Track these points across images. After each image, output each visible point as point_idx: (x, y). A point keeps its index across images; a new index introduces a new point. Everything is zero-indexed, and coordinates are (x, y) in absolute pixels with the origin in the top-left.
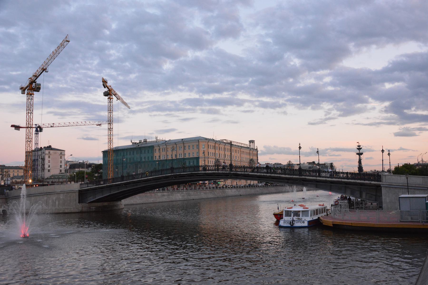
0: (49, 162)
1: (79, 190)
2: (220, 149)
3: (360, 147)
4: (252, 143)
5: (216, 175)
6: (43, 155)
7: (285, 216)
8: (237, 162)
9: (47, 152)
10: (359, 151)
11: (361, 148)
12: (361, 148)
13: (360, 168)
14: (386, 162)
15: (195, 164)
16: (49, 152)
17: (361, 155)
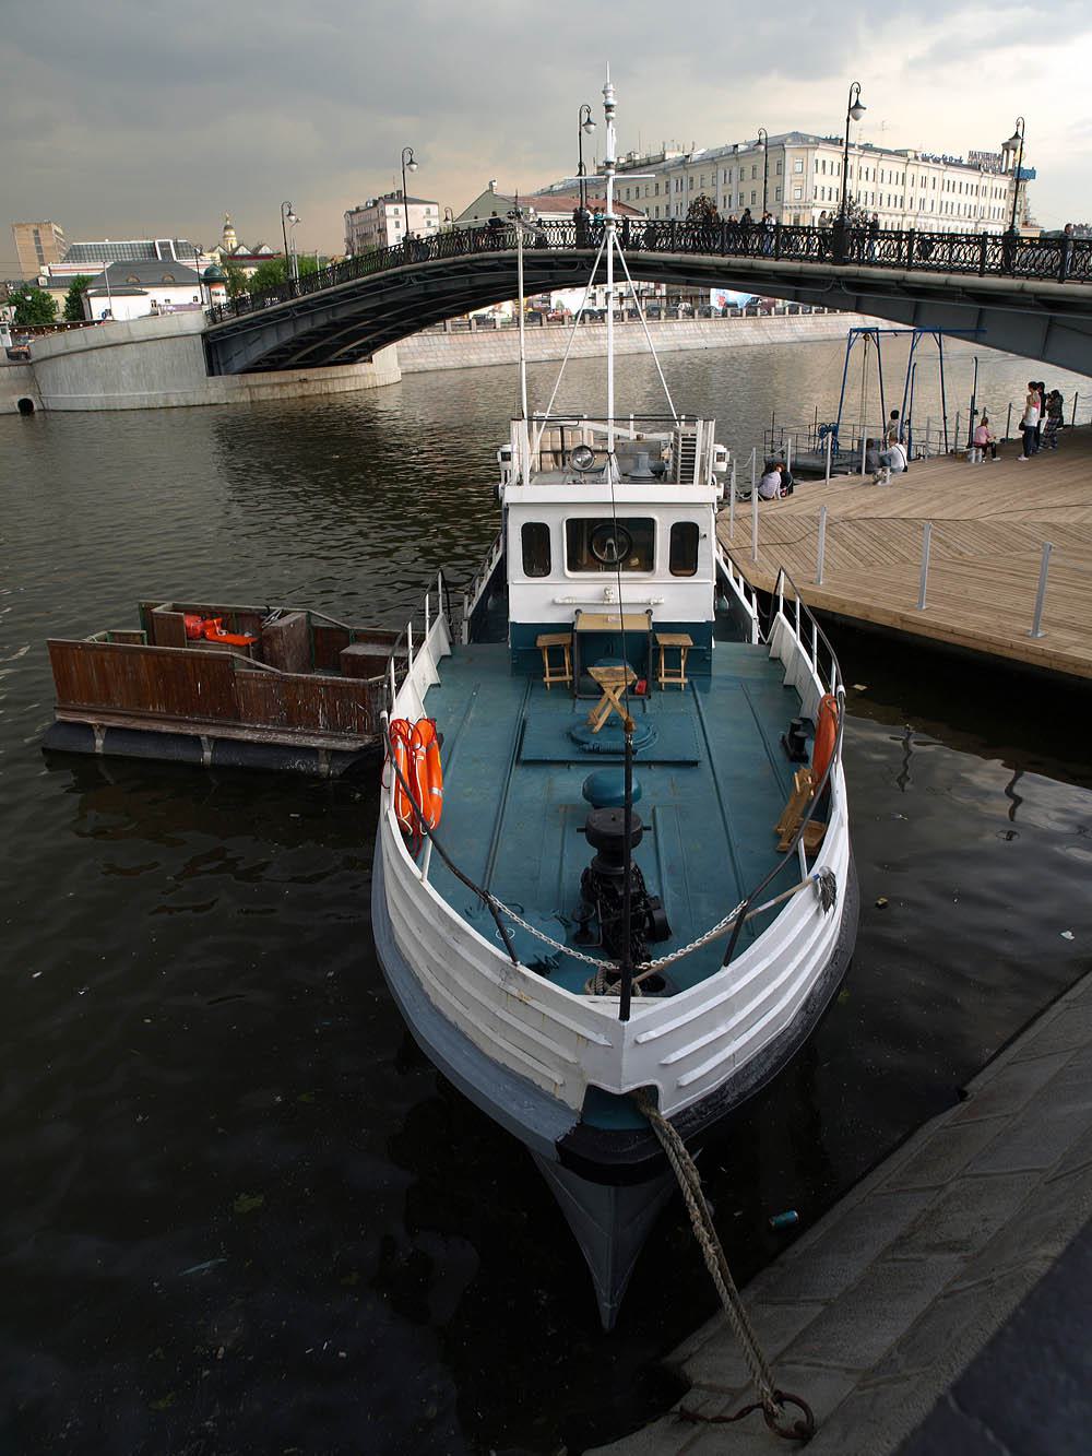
1: (204, 335)
2: (864, 176)
4: (1012, 152)
5: (479, 267)
9: (390, 209)
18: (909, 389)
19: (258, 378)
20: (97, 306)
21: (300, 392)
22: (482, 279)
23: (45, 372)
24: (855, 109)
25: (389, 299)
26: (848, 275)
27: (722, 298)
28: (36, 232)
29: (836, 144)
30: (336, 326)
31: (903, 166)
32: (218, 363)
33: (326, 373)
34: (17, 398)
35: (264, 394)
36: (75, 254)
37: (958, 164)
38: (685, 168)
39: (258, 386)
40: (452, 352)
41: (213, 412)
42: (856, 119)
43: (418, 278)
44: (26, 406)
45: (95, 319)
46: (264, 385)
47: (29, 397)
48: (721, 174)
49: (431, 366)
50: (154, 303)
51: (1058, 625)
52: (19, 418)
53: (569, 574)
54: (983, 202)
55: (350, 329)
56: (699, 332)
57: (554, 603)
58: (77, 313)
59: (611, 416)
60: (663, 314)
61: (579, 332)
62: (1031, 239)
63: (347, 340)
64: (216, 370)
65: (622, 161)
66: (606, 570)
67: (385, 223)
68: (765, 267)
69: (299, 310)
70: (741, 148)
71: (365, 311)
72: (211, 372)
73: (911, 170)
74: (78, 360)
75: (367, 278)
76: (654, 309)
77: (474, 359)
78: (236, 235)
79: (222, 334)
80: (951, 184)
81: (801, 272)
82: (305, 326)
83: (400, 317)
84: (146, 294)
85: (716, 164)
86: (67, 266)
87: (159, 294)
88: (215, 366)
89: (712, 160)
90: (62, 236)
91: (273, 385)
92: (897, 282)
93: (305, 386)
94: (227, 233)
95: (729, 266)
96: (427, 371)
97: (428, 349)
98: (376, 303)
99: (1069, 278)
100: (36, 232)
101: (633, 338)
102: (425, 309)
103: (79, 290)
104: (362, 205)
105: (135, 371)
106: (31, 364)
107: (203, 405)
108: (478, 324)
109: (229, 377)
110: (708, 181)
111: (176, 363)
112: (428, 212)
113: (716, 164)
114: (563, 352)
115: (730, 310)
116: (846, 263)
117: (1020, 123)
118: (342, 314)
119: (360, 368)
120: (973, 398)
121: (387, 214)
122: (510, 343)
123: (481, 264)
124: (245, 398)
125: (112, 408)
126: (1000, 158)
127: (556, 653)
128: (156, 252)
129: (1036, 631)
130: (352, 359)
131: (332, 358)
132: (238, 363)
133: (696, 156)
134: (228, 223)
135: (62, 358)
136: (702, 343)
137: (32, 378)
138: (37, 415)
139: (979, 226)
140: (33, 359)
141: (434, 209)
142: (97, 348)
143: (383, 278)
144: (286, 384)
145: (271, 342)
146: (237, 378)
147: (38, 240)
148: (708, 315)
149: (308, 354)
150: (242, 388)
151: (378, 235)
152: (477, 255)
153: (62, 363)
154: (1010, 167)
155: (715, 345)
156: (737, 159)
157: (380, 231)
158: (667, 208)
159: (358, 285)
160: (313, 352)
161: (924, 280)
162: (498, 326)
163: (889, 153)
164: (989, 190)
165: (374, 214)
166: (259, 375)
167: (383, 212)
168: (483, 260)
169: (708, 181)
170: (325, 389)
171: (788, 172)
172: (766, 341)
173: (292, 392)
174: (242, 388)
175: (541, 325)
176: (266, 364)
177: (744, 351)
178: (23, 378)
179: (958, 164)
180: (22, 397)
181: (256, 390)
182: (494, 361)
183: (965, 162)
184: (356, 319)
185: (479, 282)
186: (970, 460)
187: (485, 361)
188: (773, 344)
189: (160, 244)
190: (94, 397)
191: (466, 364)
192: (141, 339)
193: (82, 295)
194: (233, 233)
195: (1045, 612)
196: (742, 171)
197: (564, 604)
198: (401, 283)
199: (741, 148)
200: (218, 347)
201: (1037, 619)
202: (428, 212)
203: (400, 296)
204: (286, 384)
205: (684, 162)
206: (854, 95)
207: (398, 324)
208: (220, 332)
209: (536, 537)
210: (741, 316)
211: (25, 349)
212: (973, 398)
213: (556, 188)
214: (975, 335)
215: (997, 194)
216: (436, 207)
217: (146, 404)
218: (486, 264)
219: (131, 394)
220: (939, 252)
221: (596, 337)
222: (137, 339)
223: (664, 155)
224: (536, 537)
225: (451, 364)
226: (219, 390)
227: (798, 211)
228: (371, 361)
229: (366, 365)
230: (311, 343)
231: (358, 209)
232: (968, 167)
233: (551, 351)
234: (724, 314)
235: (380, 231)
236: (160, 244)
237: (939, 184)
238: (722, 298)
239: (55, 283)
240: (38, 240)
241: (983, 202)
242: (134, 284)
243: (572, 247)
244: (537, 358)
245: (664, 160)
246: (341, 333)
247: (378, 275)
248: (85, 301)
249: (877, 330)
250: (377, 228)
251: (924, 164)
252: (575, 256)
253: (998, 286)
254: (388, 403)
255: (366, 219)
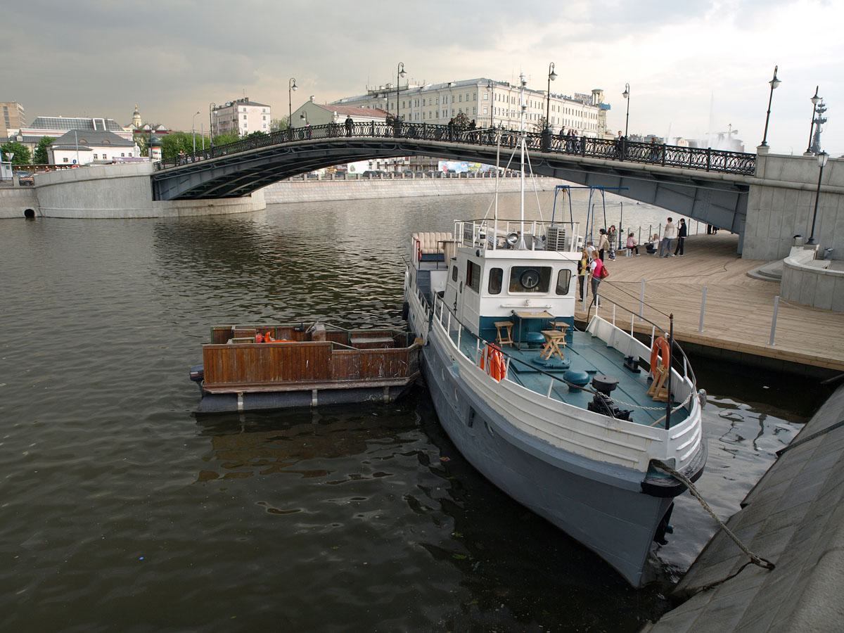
0: (246, 127)
1: (152, 176)
2: (541, 105)
3: (824, 116)
4: (597, 95)
5: (335, 145)
6: (236, 113)
7: (511, 290)
8: (515, 123)
9: (241, 108)
10: (820, 115)
11: (826, 110)
12: (825, 121)
13: (814, 148)
14: (797, 196)
15: (694, 156)
16: (245, 110)
17: (823, 123)
18: (590, 218)
19: (180, 203)
20: (59, 157)
21: (208, 212)
22: (333, 152)
23: (44, 195)
24: (552, 75)
25: (274, 161)
26: (552, 158)
27: (445, 167)
28: (6, 108)
29: (505, 86)
30: (237, 175)
31: (508, 92)
32: (159, 193)
33: (234, 201)
34: (24, 209)
35: (186, 213)
36: (39, 123)
37: (569, 99)
38: (421, 94)
39: (183, 208)
40: (292, 193)
41: (156, 221)
42: (553, 80)
43: (296, 150)
44: (29, 214)
45: (57, 163)
46: (187, 208)
47: (32, 208)
48: (441, 98)
49: (281, 201)
50: (96, 156)
51: (709, 327)
52: (24, 220)
53: (510, 293)
54: (585, 120)
55: (245, 177)
56: (434, 186)
57: (501, 307)
58: (43, 159)
59: (523, 222)
60: (414, 175)
61: (367, 183)
62: (608, 141)
63: (239, 184)
64: (157, 197)
65: (383, 88)
66: (526, 291)
67: (237, 116)
68: (506, 152)
69: (217, 165)
70: (452, 85)
71: (259, 167)
72: (154, 199)
73: (512, 94)
74: (68, 187)
75: (264, 148)
76: (408, 172)
77: (305, 197)
78: (141, 118)
79: (165, 176)
80: (568, 110)
81: (604, 165)
82: (219, 174)
83: (275, 172)
84: (91, 150)
85: (439, 92)
86: (32, 130)
87: (99, 151)
88: (156, 195)
89: (436, 90)
90: (23, 112)
91: (192, 208)
92: (578, 162)
93: (212, 209)
94: (135, 117)
95: (484, 151)
96: (278, 203)
97: (279, 190)
98: (267, 162)
99: (712, 169)
100: (6, 108)
101: (397, 188)
102: (291, 167)
103: (45, 147)
104: (223, 105)
105: (107, 196)
106: (35, 189)
107: (149, 218)
108: (395, 176)
109: (166, 201)
110: (434, 102)
111: (133, 192)
112: (264, 111)
113: (439, 92)
114: (358, 195)
115: (450, 174)
116: (549, 151)
117: (627, 86)
118: (244, 168)
119: (244, 200)
120: (620, 223)
121: (239, 111)
122: (326, 189)
123: (335, 144)
124: (175, 214)
125: (89, 217)
126: (591, 98)
127: (504, 330)
128: (93, 125)
129: (700, 329)
130: (240, 194)
131: (228, 194)
132: (173, 194)
133: (426, 88)
134: (137, 111)
135: (57, 186)
136: (436, 192)
137: (35, 197)
138: (37, 219)
139: (584, 133)
140: (37, 186)
141: (268, 110)
142: (82, 181)
143: (274, 149)
144: (201, 207)
145: (196, 182)
146: (170, 202)
147: (6, 113)
148: (439, 177)
149: (214, 191)
150: (172, 208)
151: (233, 123)
152: (334, 139)
153: (58, 189)
154: (597, 103)
155: (443, 193)
156: (450, 91)
157: (234, 120)
158: (410, 115)
159: (258, 152)
160: (217, 190)
161: (593, 162)
162: (320, 178)
163: (534, 92)
164: (588, 114)
165: (231, 110)
166: (184, 201)
167: (237, 110)
168: (337, 141)
169: (434, 102)
170: (223, 212)
171: (480, 98)
172: (472, 192)
173: (204, 212)
174: (172, 208)
175: (331, 179)
176: (188, 195)
177: (459, 197)
178: (28, 196)
179: (569, 99)
180: (28, 208)
181: (182, 210)
182: (318, 198)
183: (573, 99)
184: (249, 171)
185: (332, 153)
186: (625, 255)
187: (311, 199)
188: (476, 194)
189: (96, 121)
190: (78, 210)
191: (301, 200)
192: (111, 177)
193: (48, 149)
194: (139, 117)
195: (705, 322)
196: (453, 97)
197: (506, 308)
198: (284, 152)
199: (452, 85)
200: (159, 184)
201: (701, 325)
202: (264, 111)
203: (283, 159)
204: (201, 207)
205: (420, 90)
206: (552, 68)
207: (273, 175)
208: (163, 175)
209: (496, 275)
210: (458, 177)
211: (30, 179)
212: (620, 223)
213: (344, 101)
214: (619, 190)
215: (592, 116)
216: (269, 108)
217: (112, 216)
218: (339, 144)
219: (102, 209)
220: (670, 156)
221: (375, 187)
222: (109, 177)
223: (407, 86)
224: (496, 275)
225: (292, 200)
226: (161, 210)
227: (486, 120)
228: (250, 196)
229: (248, 198)
230: (219, 184)
231: (220, 107)
232: (576, 101)
233: (350, 194)
234: (448, 176)
235: (234, 120)
236: (96, 121)
237: (561, 109)
238: (445, 167)
239: (31, 140)
240: (6, 113)
241: (585, 120)
242: (83, 144)
243: (367, 136)
244: (342, 198)
245: (407, 89)
246: (238, 179)
247: (270, 147)
248: (49, 152)
249: (569, 187)
250: (233, 119)
251: (559, 100)
252: (394, 142)
253: (630, 166)
254: (260, 222)
255: (227, 114)
